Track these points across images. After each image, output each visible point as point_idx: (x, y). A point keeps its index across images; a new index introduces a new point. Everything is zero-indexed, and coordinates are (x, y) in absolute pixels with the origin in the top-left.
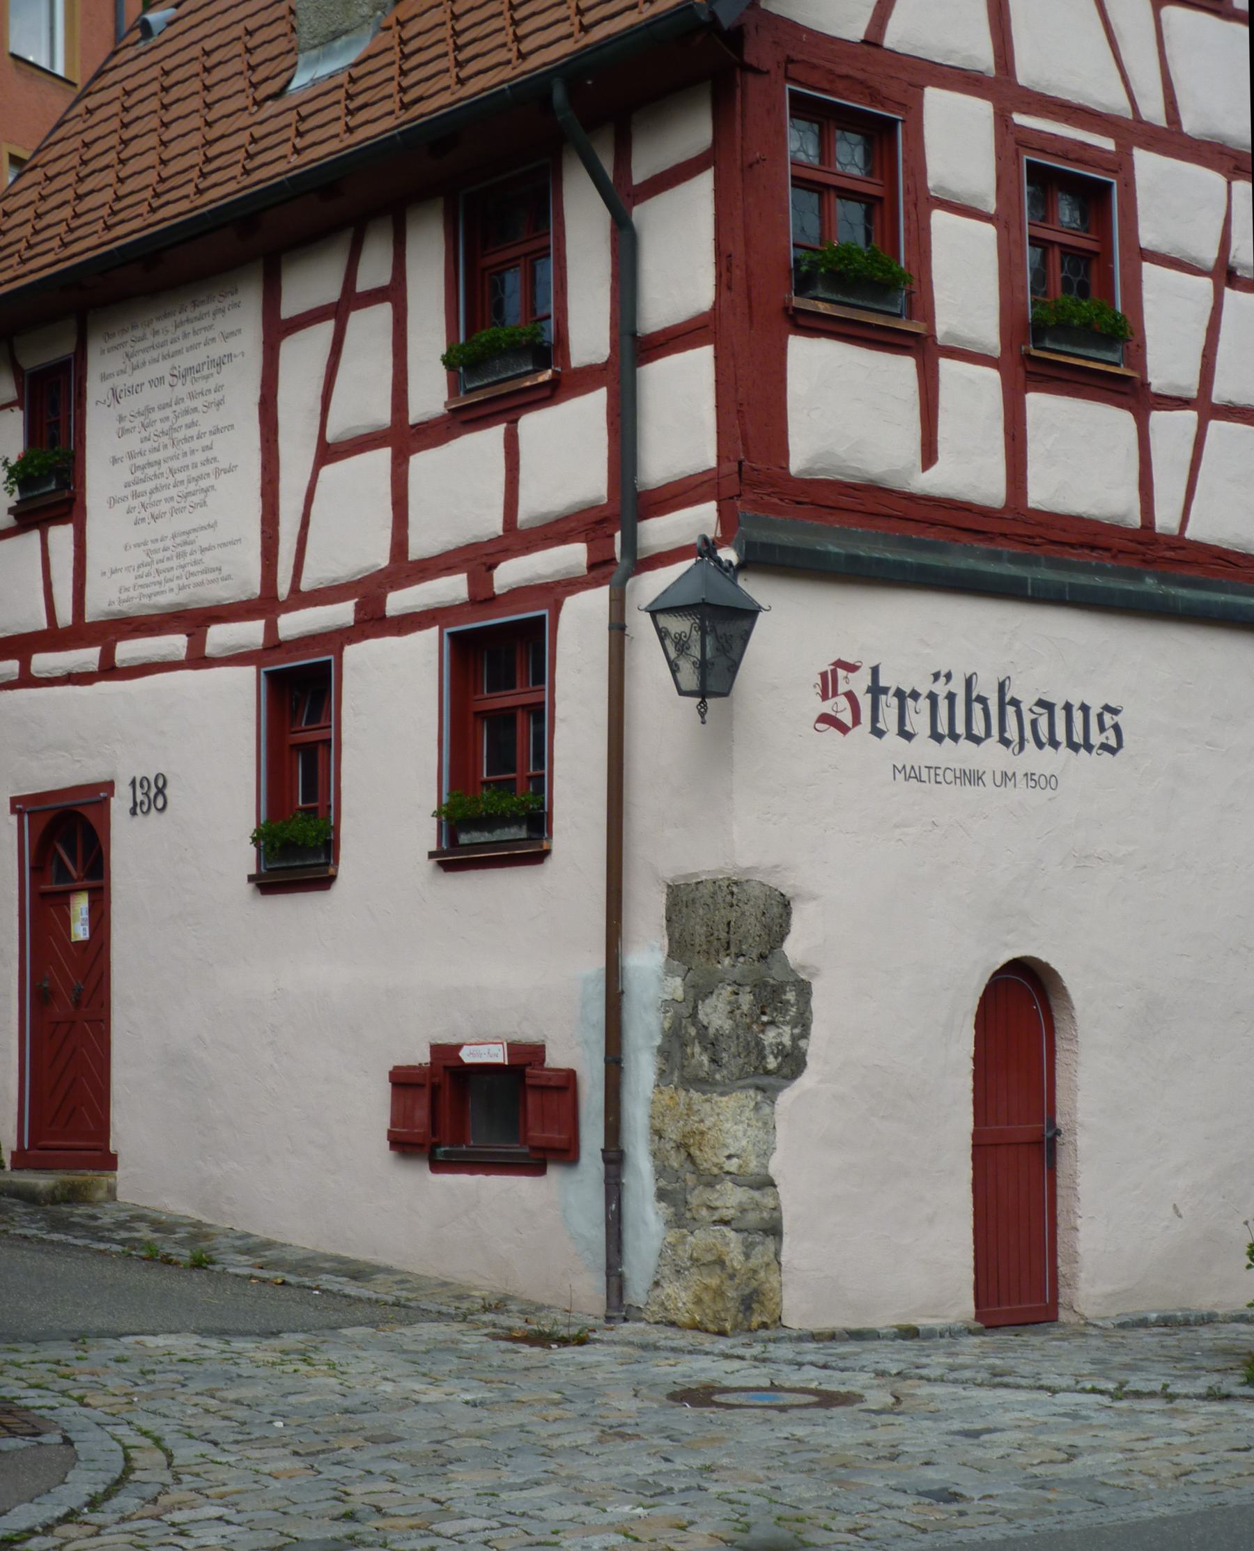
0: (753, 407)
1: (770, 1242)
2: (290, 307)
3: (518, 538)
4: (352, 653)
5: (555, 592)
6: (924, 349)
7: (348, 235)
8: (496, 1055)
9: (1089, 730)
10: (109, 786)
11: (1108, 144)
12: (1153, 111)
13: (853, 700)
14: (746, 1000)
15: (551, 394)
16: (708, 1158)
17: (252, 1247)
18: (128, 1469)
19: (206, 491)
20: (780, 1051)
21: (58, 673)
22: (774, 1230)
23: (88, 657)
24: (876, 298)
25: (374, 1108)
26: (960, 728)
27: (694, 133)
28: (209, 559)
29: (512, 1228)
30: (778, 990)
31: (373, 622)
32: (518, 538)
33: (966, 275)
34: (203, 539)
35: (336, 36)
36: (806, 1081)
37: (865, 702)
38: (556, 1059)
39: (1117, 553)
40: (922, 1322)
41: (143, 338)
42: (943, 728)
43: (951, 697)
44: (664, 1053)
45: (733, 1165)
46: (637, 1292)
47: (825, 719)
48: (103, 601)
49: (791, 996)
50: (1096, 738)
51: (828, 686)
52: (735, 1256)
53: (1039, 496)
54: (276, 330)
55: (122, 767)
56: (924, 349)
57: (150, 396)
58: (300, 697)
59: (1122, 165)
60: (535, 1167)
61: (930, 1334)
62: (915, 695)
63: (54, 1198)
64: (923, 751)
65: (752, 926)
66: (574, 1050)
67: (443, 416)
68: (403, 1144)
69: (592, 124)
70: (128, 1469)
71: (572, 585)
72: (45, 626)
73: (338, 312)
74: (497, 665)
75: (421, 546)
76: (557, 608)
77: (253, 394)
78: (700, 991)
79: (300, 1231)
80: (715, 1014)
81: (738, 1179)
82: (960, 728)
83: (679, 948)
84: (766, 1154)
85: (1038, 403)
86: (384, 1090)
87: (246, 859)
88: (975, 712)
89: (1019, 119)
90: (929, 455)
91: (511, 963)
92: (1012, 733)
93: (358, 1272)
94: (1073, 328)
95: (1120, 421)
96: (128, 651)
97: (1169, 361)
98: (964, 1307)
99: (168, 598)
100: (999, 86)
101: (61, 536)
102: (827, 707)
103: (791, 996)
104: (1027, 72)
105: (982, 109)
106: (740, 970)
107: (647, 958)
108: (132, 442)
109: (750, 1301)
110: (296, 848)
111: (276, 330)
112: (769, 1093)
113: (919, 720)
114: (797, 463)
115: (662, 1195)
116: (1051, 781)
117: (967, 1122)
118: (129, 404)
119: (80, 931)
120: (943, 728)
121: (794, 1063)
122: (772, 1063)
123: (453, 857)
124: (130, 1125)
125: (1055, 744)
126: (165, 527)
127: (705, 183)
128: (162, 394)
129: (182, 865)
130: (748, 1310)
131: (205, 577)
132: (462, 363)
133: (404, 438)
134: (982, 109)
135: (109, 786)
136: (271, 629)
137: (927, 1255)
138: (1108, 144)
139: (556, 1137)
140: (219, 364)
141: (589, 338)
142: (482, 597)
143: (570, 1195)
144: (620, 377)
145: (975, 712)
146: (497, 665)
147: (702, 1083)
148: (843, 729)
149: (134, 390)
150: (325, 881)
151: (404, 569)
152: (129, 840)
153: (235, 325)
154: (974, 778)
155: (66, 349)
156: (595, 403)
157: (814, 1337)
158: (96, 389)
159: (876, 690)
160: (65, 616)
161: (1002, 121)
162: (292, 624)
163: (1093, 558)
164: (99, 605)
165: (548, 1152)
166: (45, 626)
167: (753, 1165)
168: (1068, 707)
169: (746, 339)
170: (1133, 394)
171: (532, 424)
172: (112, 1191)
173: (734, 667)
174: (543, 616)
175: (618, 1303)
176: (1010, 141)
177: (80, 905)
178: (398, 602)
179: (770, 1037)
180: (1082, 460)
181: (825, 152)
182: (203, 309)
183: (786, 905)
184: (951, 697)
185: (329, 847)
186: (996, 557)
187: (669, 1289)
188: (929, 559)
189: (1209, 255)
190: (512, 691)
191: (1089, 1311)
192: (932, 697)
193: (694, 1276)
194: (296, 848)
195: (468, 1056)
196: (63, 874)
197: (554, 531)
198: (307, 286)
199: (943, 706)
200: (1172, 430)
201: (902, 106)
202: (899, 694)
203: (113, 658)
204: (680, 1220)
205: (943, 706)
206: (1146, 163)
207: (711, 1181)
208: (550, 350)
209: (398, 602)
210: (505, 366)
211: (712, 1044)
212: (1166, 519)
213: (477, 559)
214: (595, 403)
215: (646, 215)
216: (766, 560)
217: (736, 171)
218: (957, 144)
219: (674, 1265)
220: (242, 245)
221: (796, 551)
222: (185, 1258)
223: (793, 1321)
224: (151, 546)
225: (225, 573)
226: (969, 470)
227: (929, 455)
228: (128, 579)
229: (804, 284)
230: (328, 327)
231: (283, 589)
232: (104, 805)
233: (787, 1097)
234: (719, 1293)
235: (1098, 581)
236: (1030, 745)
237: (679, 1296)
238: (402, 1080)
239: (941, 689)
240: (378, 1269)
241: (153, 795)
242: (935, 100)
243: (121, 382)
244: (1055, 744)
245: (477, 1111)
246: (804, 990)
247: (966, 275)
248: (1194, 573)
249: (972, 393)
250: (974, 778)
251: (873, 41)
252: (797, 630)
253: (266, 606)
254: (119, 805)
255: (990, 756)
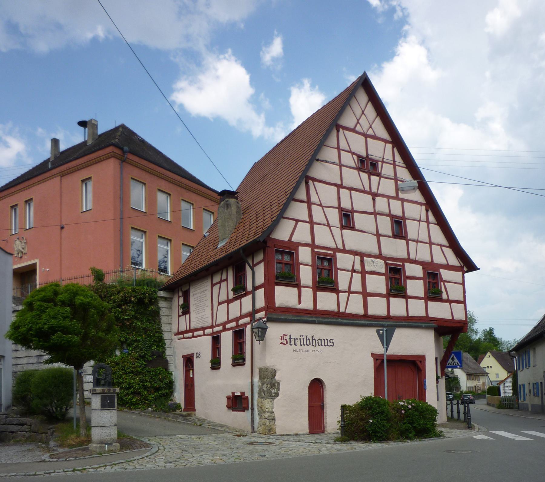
0: (270, 297)
1: (274, 421)
3: (242, 317)
5: (245, 325)
6: (298, 286)
7: (221, 272)
8: (239, 394)
9: (328, 343)
10: (193, 354)
11: (332, 252)
12: (340, 246)
13: (286, 340)
14: (269, 385)
15: (245, 295)
16: (264, 409)
17: (210, 423)
18: (159, 449)
20: (275, 393)
22: (274, 419)
23: (190, 334)
24: (290, 279)
25: (225, 402)
26: (305, 344)
27: (261, 257)
28: (205, 320)
29: (240, 419)
30: (274, 384)
31: (225, 329)
32: (242, 317)
33: (306, 275)
34: (204, 317)
35: (224, 239)
36: (279, 397)
37: (288, 341)
38: (246, 395)
39: (333, 316)
40: (299, 433)
42: (302, 344)
43: (303, 339)
44: (259, 393)
45: (267, 410)
46: (256, 429)
47: (281, 343)
48: (193, 326)
49: (276, 385)
50: (329, 344)
51: (282, 338)
52: (268, 424)
53: (319, 308)
54: (213, 285)
55: (195, 351)
56: (298, 286)
57: (198, 295)
58: (216, 340)
59: (334, 256)
60: (244, 411)
61: (300, 435)
62: (297, 339)
63: (186, 416)
64: (299, 347)
65: (270, 374)
66: (248, 394)
68: (228, 407)
69: (247, 256)
70: (159, 449)
71: (248, 324)
73: (220, 283)
74: (239, 334)
75: (230, 318)
76: (246, 327)
77: (210, 295)
78: (263, 384)
79: (217, 421)
80: (264, 388)
81: (268, 412)
82: (305, 344)
83: (260, 378)
84: (273, 408)
85: (318, 293)
86: (225, 400)
87: (210, 365)
88: (306, 341)
89: (315, 250)
90: (300, 302)
91: (237, 380)
92: (314, 344)
93: (222, 426)
94: (325, 281)
95: (334, 295)
96: (196, 333)
97: (343, 284)
98: (307, 431)
99: (200, 325)
100: (313, 245)
101: (188, 316)
102: (282, 341)
103: (276, 385)
104: (317, 243)
105: (309, 249)
106: (269, 382)
107: (256, 379)
108: (196, 302)
109: (270, 430)
110: (216, 364)
111: (213, 285)
112: (273, 399)
113: (298, 342)
114: (277, 305)
115: (259, 414)
116: (321, 351)
117: (307, 403)
118: (196, 296)
119: (191, 376)
120: (302, 344)
121: (277, 395)
122: (273, 395)
123: (234, 365)
124: (198, 404)
125: (322, 345)
126: (200, 315)
127: (263, 264)
128: (199, 295)
129: (203, 364)
130: (270, 431)
132: (235, 290)
133: (229, 302)
134: (309, 249)
135: (193, 354)
136: (213, 330)
137: (302, 423)
138: (332, 252)
139: (246, 406)
141: (249, 288)
142: (237, 326)
143: (247, 415)
144: (253, 293)
145: (306, 341)
146: (239, 334)
147: (263, 398)
148: (285, 344)
149: (196, 294)
150: (219, 368)
151: (229, 321)
152: (196, 361)
154: (308, 351)
155: (188, 288)
156: (250, 296)
157: (280, 435)
158: (191, 294)
159: (290, 338)
160: (188, 328)
161: (313, 251)
162: (215, 329)
163: (329, 316)
164: (192, 327)
165: (244, 409)
167: (270, 410)
168: (324, 340)
169: (269, 288)
170: (336, 291)
171: (243, 299)
172: (195, 414)
173: (264, 337)
175: (253, 430)
176: (314, 253)
177: (191, 372)
178: (228, 326)
179: (273, 391)
180: (327, 301)
181: (283, 258)
183: (275, 371)
184: (303, 339)
185: (219, 363)
186: (312, 317)
187: (260, 428)
188: (299, 318)
189: (350, 268)
191: (329, 431)
192: (300, 339)
193: (263, 426)
194: (216, 364)
195: (236, 394)
196: (189, 367)
197: (246, 316)
198: (217, 279)
199: (302, 341)
200: (343, 297)
201: (294, 250)
202: (294, 339)
204: (261, 418)
205: (302, 341)
206: (338, 255)
207: (264, 412)
208: (245, 289)
209: (228, 326)
210: (240, 290)
211: (264, 392)
212: (342, 310)
213: (237, 320)
214: (250, 296)
215: (256, 268)
216: (270, 320)
217: (267, 262)
218: (305, 255)
219: (261, 425)
220: (206, 273)
221: (276, 318)
222: (201, 424)
223: (277, 433)
226: (307, 304)
227: (300, 302)
228: (195, 323)
229: (277, 278)
231: (214, 324)
232: (193, 356)
233: (276, 400)
234: (265, 429)
235: (330, 320)
236: (317, 346)
237: (261, 429)
238: (228, 398)
239: (302, 338)
240: (225, 426)
241: (199, 355)
242: (301, 248)
243: (194, 293)
244: (322, 345)
245: (237, 402)
246: (279, 384)
247: (306, 275)
248: (347, 318)
249: (307, 293)
250: (308, 351)
251: (290, 240)
252: (275, 331)
253: (212, 327)
254: (195, 357)
255: (311, 347)
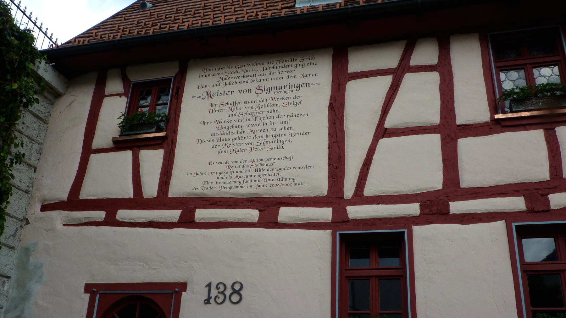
2: (414, 61)
4: (418, 230)
19: (284, 142)
21: (142, 221)
41: (237, 72)
67: (487, 123)
72: (131, 195)
96: (201, 214)
131: (280, 182)
140: (299, 87)
153: (316, 75)
166: (131, 195)
174: (516, 226)
182: (306, 62)
190: (557, 262)
203: (194, 215)
224: (231, 164)
225: (297, 181)
230: (388, 80)
251: (125, 94)
